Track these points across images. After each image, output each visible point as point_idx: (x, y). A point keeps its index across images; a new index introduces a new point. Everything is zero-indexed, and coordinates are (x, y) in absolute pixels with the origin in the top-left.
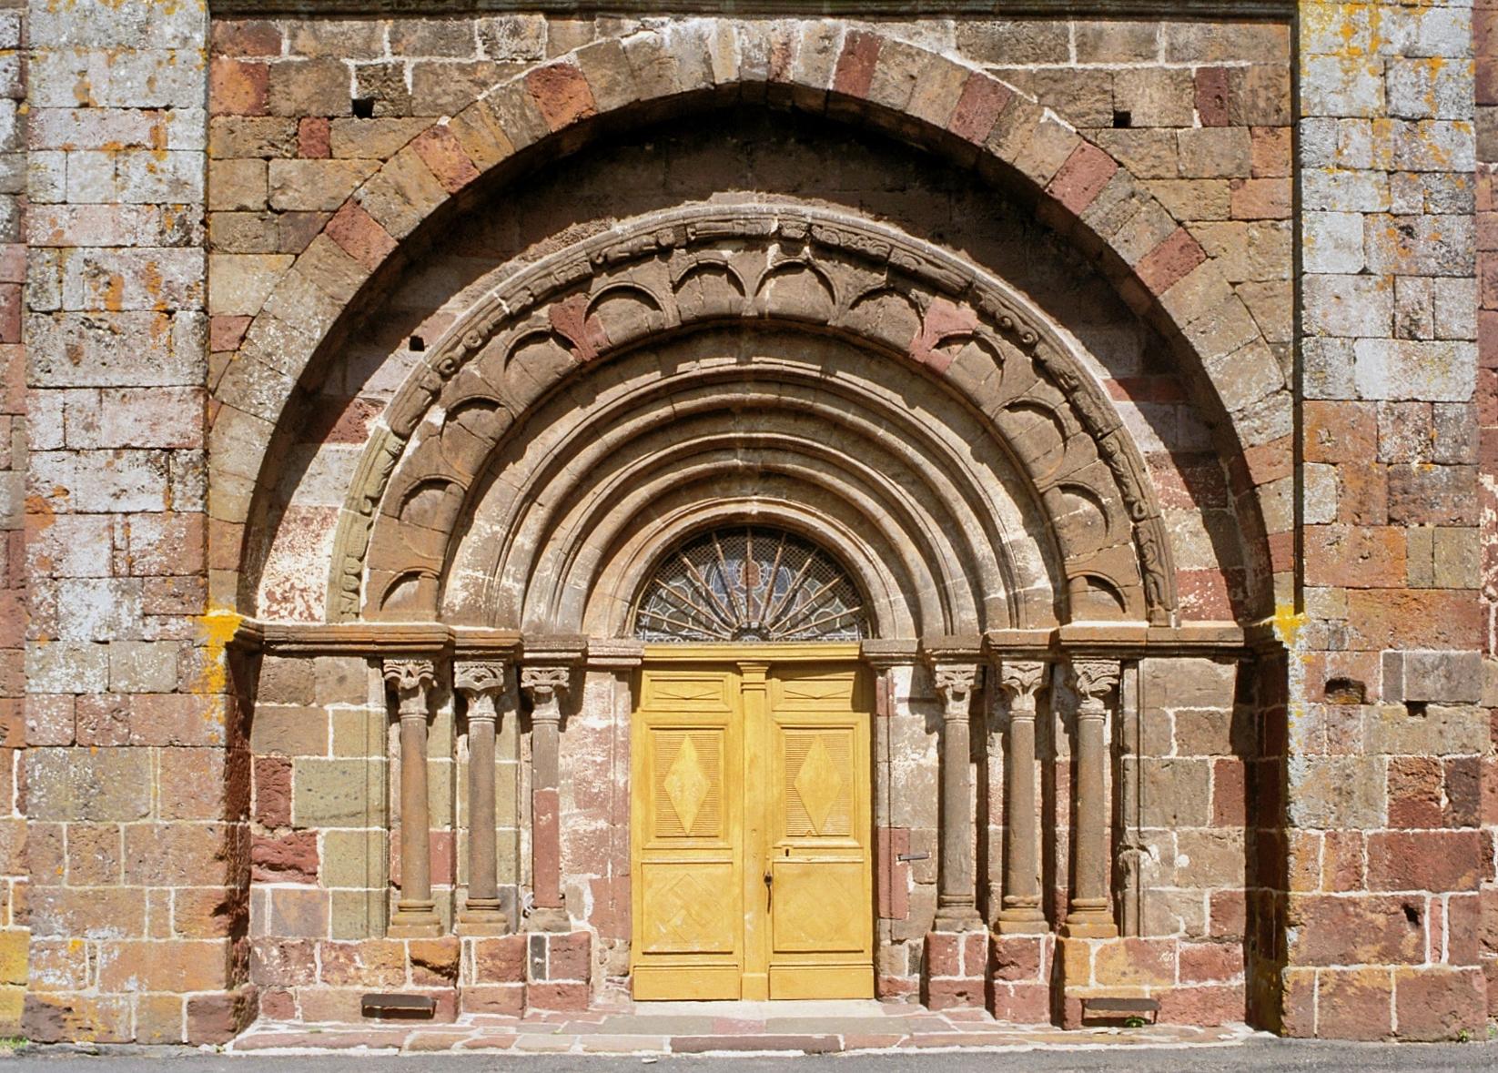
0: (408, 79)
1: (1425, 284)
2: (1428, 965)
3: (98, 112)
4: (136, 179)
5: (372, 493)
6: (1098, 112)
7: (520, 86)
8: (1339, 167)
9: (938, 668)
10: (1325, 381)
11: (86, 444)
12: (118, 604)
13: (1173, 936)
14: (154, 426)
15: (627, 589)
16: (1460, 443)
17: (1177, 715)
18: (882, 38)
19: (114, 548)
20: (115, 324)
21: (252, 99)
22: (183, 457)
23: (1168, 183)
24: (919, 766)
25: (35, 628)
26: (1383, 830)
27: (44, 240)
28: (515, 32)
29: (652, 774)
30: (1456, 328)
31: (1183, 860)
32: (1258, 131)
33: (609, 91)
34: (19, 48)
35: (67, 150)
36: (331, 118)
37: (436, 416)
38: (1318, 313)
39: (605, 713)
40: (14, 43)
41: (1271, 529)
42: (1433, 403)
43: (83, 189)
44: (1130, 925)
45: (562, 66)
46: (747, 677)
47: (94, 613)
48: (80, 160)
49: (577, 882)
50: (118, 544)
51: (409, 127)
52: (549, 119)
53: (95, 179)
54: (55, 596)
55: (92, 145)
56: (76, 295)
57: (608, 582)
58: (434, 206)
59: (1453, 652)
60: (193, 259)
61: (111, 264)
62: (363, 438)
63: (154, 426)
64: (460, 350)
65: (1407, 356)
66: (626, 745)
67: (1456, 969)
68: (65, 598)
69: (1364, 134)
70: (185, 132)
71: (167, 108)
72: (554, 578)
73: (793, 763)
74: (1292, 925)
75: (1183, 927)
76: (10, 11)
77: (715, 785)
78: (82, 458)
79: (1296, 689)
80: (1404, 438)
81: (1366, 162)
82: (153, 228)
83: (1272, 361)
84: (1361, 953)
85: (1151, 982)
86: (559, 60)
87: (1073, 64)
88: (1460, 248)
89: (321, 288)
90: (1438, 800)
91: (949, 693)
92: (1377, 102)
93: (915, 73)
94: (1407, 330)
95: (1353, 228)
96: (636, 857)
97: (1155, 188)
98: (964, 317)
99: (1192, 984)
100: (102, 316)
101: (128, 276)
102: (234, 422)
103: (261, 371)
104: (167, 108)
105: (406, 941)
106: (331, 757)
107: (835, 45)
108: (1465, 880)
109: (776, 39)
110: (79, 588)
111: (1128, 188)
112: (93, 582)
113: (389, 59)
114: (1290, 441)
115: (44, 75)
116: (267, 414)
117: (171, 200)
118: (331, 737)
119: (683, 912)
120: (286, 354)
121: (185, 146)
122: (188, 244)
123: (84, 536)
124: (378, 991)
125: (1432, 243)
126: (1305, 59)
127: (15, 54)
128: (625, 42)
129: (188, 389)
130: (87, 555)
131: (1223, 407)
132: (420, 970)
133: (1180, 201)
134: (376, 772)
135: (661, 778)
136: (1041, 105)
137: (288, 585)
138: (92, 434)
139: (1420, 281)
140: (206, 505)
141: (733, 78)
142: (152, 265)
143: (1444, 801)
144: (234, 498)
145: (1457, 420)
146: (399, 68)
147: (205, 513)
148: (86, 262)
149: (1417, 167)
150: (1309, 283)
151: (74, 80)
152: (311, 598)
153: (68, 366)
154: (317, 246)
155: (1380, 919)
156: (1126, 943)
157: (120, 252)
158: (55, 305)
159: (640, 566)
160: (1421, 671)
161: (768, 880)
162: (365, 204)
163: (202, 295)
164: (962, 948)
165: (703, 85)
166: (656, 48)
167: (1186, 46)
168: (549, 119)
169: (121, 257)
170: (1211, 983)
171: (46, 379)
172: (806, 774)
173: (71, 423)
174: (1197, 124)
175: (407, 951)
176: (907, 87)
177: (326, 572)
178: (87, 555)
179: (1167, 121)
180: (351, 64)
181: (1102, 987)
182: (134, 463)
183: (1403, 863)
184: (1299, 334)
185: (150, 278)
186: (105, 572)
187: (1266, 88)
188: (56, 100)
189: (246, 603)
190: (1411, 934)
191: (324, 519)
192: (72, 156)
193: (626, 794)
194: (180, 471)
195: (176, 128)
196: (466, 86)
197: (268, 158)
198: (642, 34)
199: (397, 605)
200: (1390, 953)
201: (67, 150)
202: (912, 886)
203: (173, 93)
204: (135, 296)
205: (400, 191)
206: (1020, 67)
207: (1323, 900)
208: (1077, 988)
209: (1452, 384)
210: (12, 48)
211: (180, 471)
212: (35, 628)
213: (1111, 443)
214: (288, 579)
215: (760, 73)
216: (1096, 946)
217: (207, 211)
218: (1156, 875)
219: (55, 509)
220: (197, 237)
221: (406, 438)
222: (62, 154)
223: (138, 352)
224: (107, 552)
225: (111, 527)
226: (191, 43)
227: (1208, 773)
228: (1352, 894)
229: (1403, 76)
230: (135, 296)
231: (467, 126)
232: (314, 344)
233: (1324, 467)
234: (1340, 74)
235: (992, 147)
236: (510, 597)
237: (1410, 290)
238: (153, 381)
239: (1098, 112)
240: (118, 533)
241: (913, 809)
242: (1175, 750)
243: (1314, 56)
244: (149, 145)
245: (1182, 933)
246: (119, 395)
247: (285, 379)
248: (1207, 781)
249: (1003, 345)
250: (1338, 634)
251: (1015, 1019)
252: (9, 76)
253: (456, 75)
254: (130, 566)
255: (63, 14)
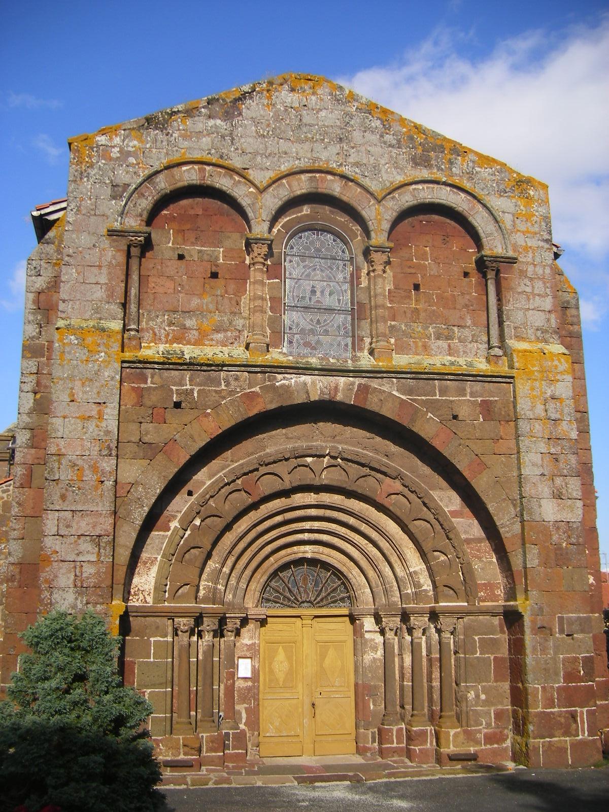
0: (196, 395)
1: (564, 480)
2: (581, 737)
3: (78, 404)
4: (91, 430)
5: (173, 553)
6: (447, 415)
7: (238, 399)
8: (531, 436)
9: (383, 620)
10: (531, 514)
11: (66, 533)
12: (76, 599)
13: (481, 727)
14: (94, 527)
15: (259, 587)
16: (578, 537)
17: (478, 638)
18: (370, 386)
19: (76, 575)
20: (81, 485)
21: (135, 401)
22: (105, 539)
23: (472, 441)
24: (374, 658)
25: (42, 608)
26: (561, 684)
27: (53, 452)
28: (236, 379)
29: (267, 662)
30: (574, 494)
31: (483, 697)
32: (502, 422)
33: (271, 402)
34: (37, 373)
35: (64, 417)
36: (165, 409)
37: (197, 522)
38: (528, 490)
39: (251, 638)
40: (35, 372)
41: (514, 568)
42: (568, 522)
43: (70, 432)
44: (464, 724)
45: (254, 392)
46: (304, 622)
47: (66, 602)
48: (69, 421)
49: (241, 708)
50: (78, 574)
51: (196, 413)
52: (248, 411)
53: (75, 429)
54: (51, 595)
55: (74, 416)
56: (65, 474)
57: (253, 586)
58: (204, 443)
59: (581, 615)
60: (112, 461)
61: (80, 462)
62: (168, 530)
63: (94, 527)
64: (208, 496)
65: (559, 505)
66: (259, 651)
67: (591, 738)
68: (55, 596)
69: (540, 425)
70: (111, 412)
71: (104, 403)
72: (235, 584)
73: (323, 656)
74: (530, 723)
75: (484, 723)
76: (35, 359)
77: (292, 666)
78: (65, 539)
79: (527, 630)
80: (560, 535)
81: (540, 435)
82: (97, 448)
83: (511, 506)
84: (556, 733)
85: (473, 746)
86: (253, 390)
87: (438, 397)
88: (574, 466)
89: (160, 473)
90: (580, 672)
91: (387, 629)
92: (543, 414)
93: (382, 399)
94: (558, 496)
95: (537, 458)
96: (261, 696)
97: (468, 442)
98: (397, 486)
99: (488, 746)
100: (75, 482)
101: (86, 467)
102: (125, 525)
103: (135, 505)
104: (104, 403)
105: (181, 737)
106: (152, 660)
107: (354, 388)
108: (591, 703)
109: (333, 385)
110: (60, 592)
111: (459, 442)
112: (66, 589)
113: (188, 387)
114: (520, 536)
115: (57, 389)
116: (137, 522)
117: (104, 438)
118: (152, 651)
119: (279, 720)
120: (146, 498)
121: (111, 418)
122: (110, 455)
123: (63, 571)
124: (169, 758)
125: (565, 464)
126: (518, 398)
127: (35, 375)
128: (277, 384)
129: (108, 512)
130: (65, 579)
131: (495, 523)
132: (186, 749)
133: (477, 447)
134: (170, 666)
135: (270, 664)
136: (427, 412)
137: (137, 588)
138: (69, 529)
139: (561, 478)
140: (113, 559)
141: (317, 399)
142: (97, 462)
143: (582, 672)
144: (124, 555)
145: (577, 528)
146: (192, 390)
147: (113, 562)
148: (70, 461)
149: (558, 437)
150: (524, 478)
151: (69, 391)
152: (146, 594)
153: (60, 502)
154: (159, 457)
155: (563, 720)
156: (463, 730)
157: (84, 457)
158: (57, 477)
159: (265, 578)
160: (571, 622)
161: (313, 705)
162: (178, 441)
163: (115, 475)
164: (395, 733)
165: (306, 401)
166: (289, 387)
167: (477, 392)
168: (248, 411)
169: (84, 460)
170: (496, 746)
171: (52, 507)
172: (327, 662)
173: (61, 525)
174: (481, 420)
175: (181, 741)
176: (379, 404)
177: (153, 584)
178: (65, 579)
179: (471, 418)
180: (174, 388)
181: (455, 749)
182: (85, 541)
183: (570, 697)
184: (522, 497)
185: (94, 468)
186: (71, 586)
187: (504, 407)
188: (61, 398)
189: (126, 600)
190: (574, 726)
191: (152, 562)
192: (66, 420)
193: (259, 671)
194: (104, 545)
195: (108, 411)
196: (217, 398)
197: (141, 423)
198: (283, 382)
199: (179, 597)
200: (567, 733)
201: (64, 417)
202: (372, 707)
203: (107, 398)
204: (89, 476)
205: (192, 437)
206: (419, 398)
207: (541, 712)
208: (446, 750)
209: (575, 515)
210: (34, 373)
211: (104, 545)
212: (42, 608)
213: (451, 535)
214: (137, 586)
215: (327, 397)
216: (452, 732)
217: (118, 443)
218: (474, 703)
219: (53, 559)
220: (114, 453)
221: (186, 530)
222: (63, 419)
223: (89, 497)
224: (72, 577)
225: (75, 567)
226: (115, 379)
227: (491, 662)
228: (552, 710)
229: (551, 405)
230: (89, 476)
231: (218, 414)
232: (157, 495)
233: (533, 546)
234: (530, 404)
235: (411, 427)
236: (221, 592)
237: (559, 481)
238: (95, 509)
239: (447, 415)
240: (78, 570)
241: (372, 675)
242: (478, 653)
243: (521, 398)
244: (97, 417)
245: (484, 726)
246: (81, 514)
247: (145, 508)
248: (491, 665)
249: (412, 497)
250: (541, 609)
251: (419, 762)
252: (32, 384)
253: (214, 394)
254: (82, 583)
255: (66, 366)
